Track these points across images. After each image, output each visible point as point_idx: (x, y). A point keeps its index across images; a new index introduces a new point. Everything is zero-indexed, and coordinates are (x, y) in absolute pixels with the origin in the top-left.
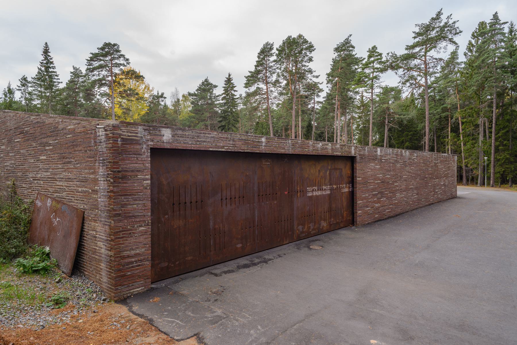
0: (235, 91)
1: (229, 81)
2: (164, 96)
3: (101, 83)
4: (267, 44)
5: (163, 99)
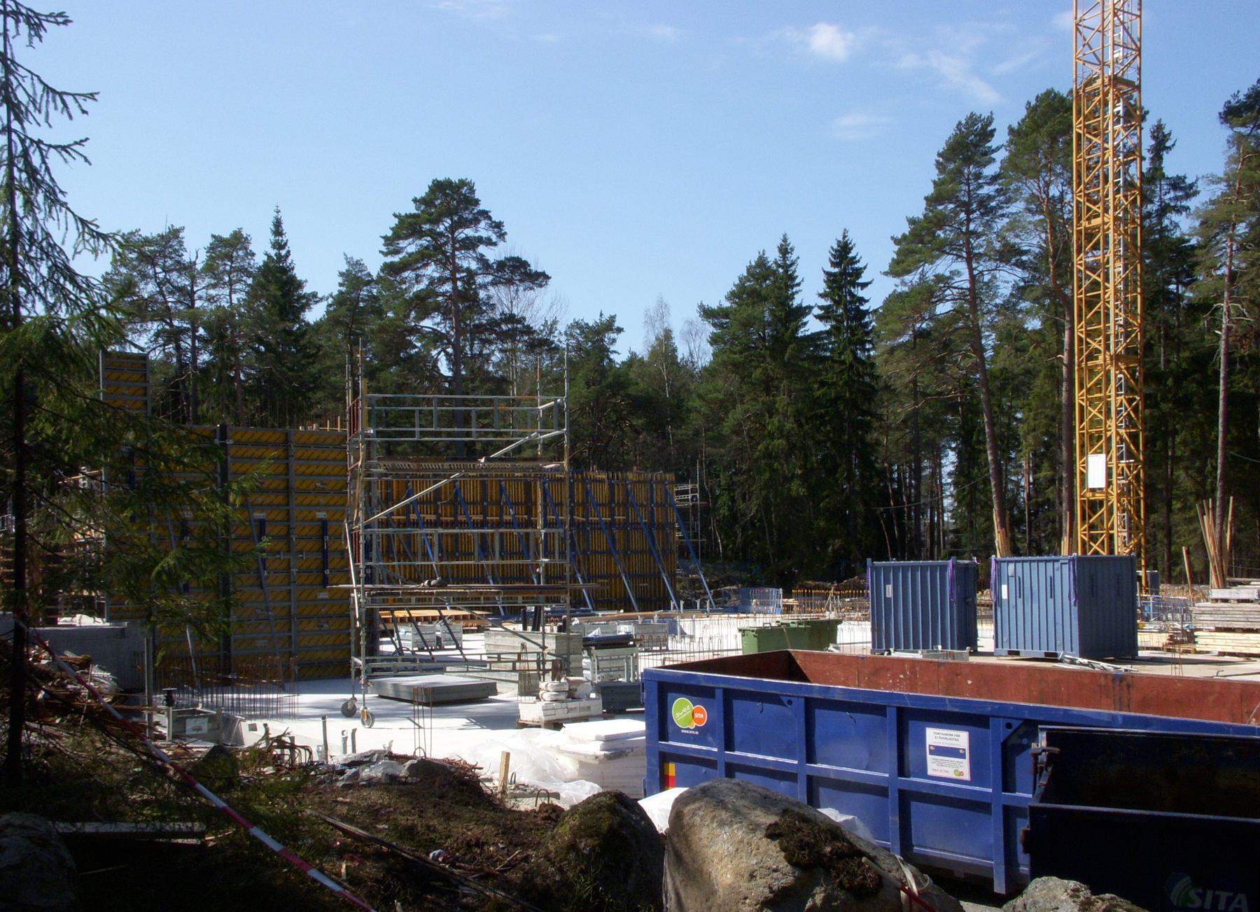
0: (864, 285)
1: (843, 253)
2: (616, 325)
3: (423, 304)
4: (972, 119)
5: (613, 335)
